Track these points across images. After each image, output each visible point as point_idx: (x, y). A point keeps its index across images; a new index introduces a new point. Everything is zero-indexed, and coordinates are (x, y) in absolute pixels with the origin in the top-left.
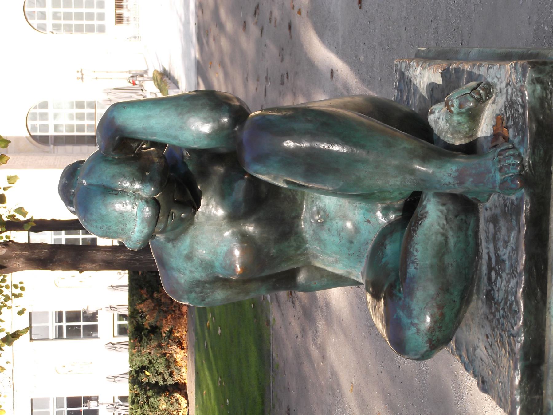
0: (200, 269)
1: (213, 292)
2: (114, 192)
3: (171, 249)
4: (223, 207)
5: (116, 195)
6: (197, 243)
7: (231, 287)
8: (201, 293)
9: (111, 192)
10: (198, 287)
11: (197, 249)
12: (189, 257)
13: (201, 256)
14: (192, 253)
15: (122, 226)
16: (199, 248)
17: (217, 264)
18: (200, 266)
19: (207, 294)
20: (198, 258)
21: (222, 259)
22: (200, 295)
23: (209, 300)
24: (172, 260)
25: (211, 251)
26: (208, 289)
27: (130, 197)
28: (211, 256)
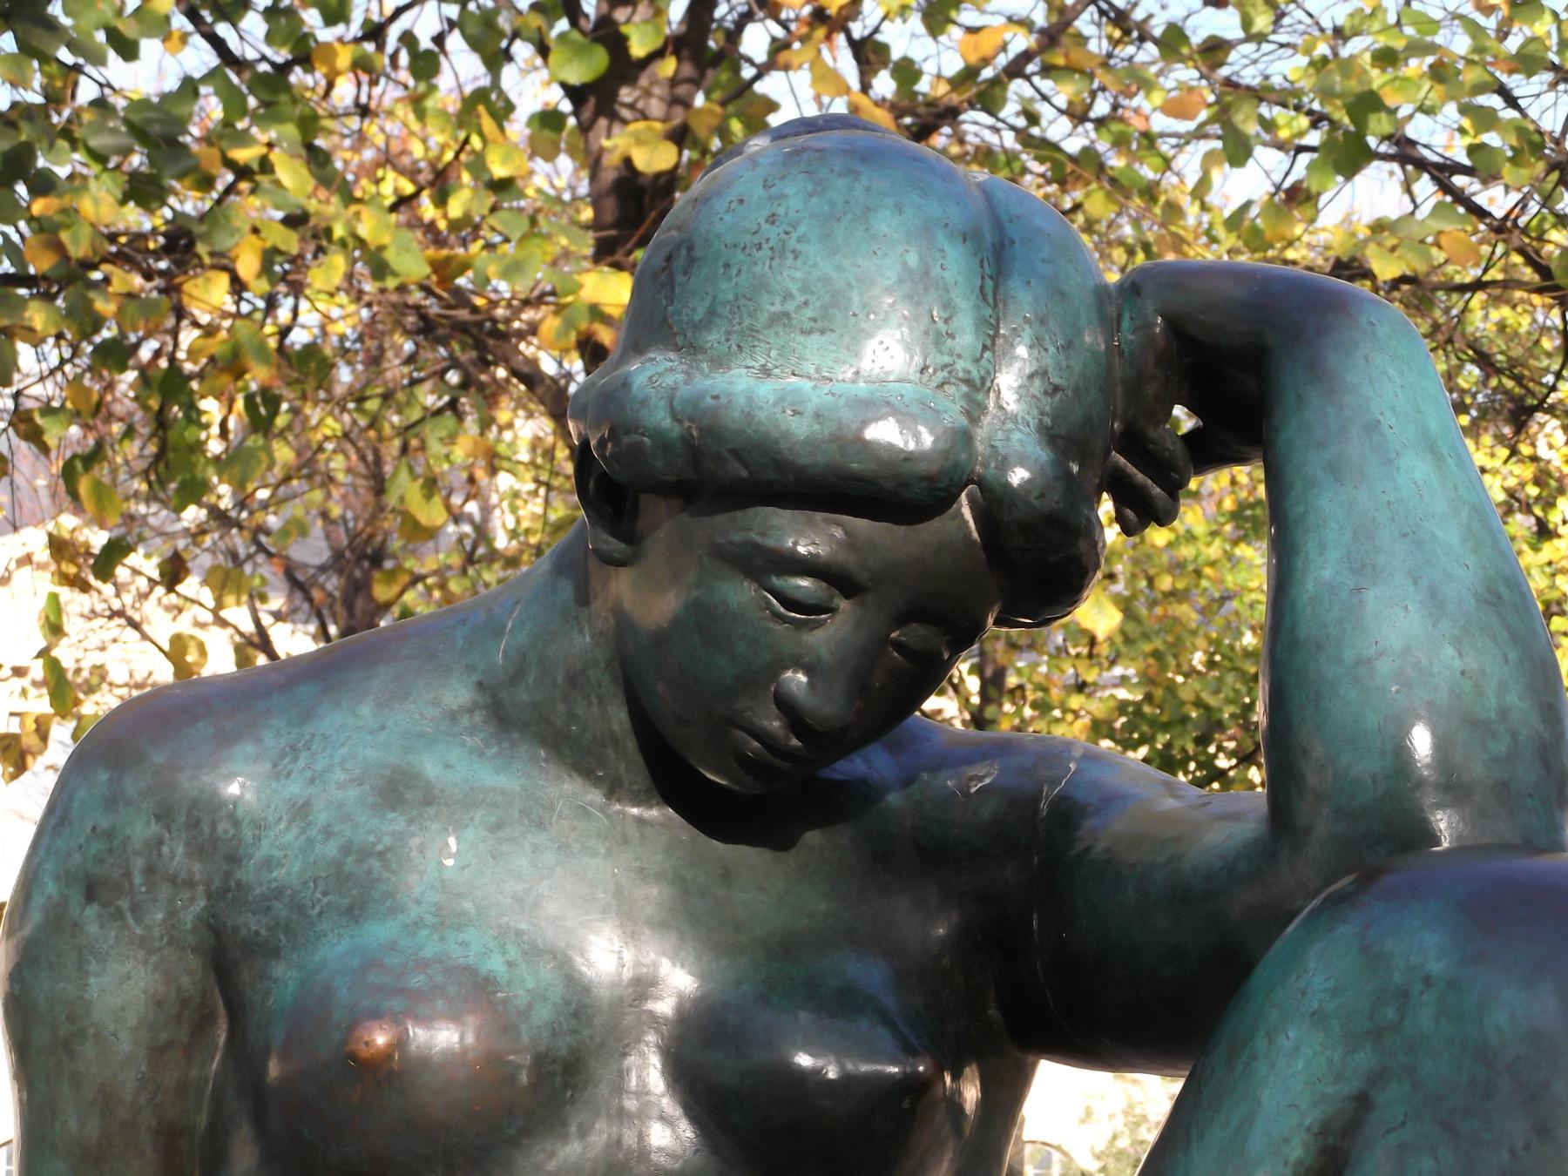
0: (331, 850)
1: (143, 942)
2: (989, 284)
3: (435, 703)
4: (478, 1037)
5: (982, 288)
6: (498, 826)
7: (157, 1053)
8: (150, 870)
9: (988, 271)
10: (200, 850)
11: (459, 827)
12: (398, 791)
13: (422, 849)
14: (429, 800)
15: (809, 313)
16: (470, 834)
17: (378, 932)
18: (346, 849)
19: (136, 909)
20: (401, 836)
21: (429, 951)
22: (138, 864)
23: (93, 929)
24: (365, 710)
25: (458, 895)
26: (172, 913)
27: (977, 361)
28: (433, 897)
